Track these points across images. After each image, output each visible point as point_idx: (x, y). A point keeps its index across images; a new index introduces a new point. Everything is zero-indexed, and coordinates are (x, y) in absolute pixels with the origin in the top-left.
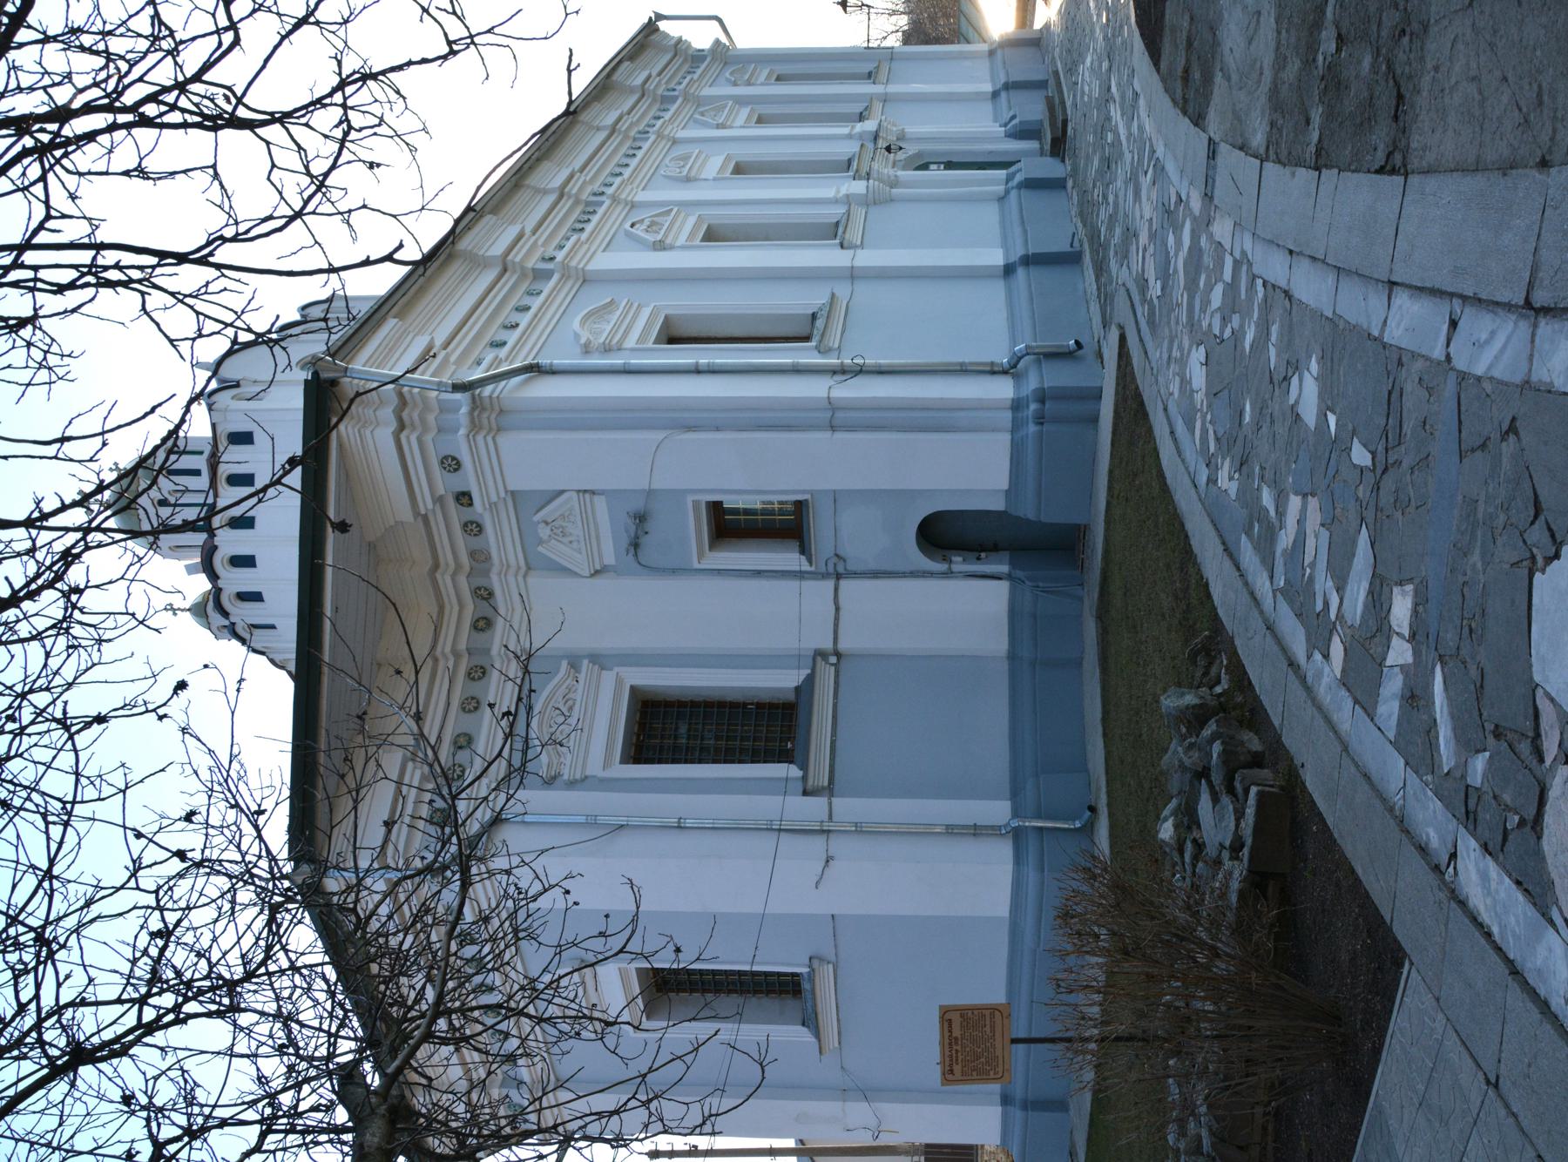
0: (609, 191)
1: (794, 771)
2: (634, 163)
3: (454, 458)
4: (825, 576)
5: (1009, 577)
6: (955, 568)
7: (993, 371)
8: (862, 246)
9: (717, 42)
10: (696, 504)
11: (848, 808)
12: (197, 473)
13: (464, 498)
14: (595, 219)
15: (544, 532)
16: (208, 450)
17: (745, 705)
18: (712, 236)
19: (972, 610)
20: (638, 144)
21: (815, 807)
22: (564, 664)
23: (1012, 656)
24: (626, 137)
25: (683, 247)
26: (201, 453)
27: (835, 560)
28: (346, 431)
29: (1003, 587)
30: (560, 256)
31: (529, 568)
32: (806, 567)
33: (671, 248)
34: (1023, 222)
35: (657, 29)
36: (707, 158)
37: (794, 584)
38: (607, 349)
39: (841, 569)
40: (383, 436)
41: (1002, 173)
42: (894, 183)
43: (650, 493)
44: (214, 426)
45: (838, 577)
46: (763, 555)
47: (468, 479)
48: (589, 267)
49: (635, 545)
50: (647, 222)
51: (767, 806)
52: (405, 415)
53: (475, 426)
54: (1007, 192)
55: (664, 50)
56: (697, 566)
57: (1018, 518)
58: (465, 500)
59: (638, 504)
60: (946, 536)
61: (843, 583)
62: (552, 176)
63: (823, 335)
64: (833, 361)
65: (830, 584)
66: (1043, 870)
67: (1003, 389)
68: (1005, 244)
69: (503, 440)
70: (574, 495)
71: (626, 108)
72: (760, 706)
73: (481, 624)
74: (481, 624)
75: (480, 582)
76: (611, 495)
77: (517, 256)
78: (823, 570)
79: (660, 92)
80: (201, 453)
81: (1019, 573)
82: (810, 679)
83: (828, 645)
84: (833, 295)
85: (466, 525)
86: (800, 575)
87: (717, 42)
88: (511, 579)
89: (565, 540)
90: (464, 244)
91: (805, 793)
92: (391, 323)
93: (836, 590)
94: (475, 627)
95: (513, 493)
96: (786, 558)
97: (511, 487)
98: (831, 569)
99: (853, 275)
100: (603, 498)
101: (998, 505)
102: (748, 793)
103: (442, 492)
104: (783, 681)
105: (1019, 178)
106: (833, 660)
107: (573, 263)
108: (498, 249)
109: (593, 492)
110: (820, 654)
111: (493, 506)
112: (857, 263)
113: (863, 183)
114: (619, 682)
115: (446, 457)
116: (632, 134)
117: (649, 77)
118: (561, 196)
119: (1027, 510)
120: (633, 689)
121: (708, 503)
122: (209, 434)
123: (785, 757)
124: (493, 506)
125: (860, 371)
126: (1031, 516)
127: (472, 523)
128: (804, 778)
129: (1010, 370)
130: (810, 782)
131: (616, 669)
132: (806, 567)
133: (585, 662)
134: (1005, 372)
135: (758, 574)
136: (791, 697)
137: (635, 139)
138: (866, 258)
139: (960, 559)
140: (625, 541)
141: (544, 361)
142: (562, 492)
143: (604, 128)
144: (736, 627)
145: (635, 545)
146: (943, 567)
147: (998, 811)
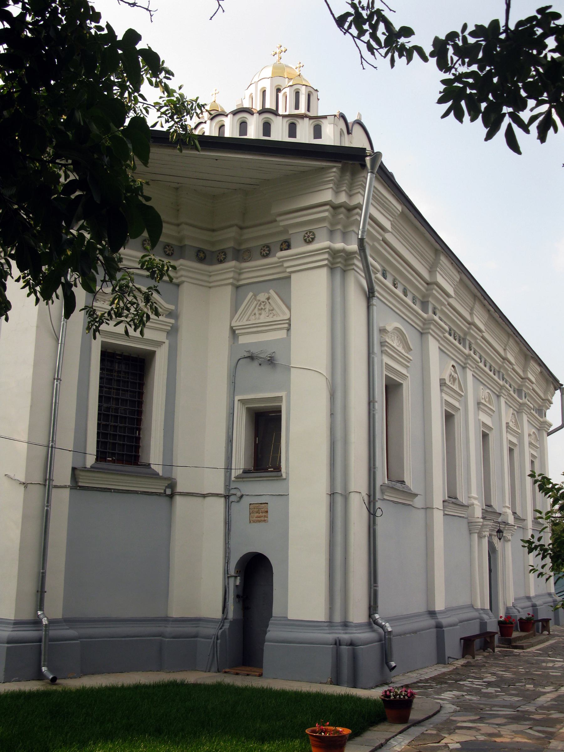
0: (472, 353)
1: (91, 460)
2: (487, 369)
3: (313, 239)
4: (227, 486)
5: (225, 619)
6: (232, 580)
7: (373, 608)
8: (445, 515)
9: (550, 425)
10: (280, 399)
11: (62, 499)
12: (297, 107)
13: (286, 245)
14: (456, 343)
15: (262, 297)
16: (311, 114)
17: (139, 429)
18: (449, 417)
19: (201, 590)
20: (497, 374)
21: (62, 475)
22: (172, 307)
23: (166, 620)
24: (500, 367)
25: (442, 398)
26: (309, 110)
27: (239, 494)
28: (334, 171)
29: (218, 615)
30: (436, 318)
31: (238, 287)
32: (234, 474)
33: (442, 391)
34: (461, 622)
35: (556, 390)
36: (490, 416)
37: (222, 464)
38: (383, 344)
39: (232, 498)
40: (327, 196)
41: (487, 607)
42: (480, 537)
43: (288, 368)
44: (325, 117)
45: (227, 497)
46: (441, 483)
47: (298, 249)
48: (430, 338)
49: (252, 358)
50: (456, 376)
51: (66, 438)
52: (343, 210)
53: (334, 254)
54: (477, 610)
55: (545, 393)
56: (237, 398)
57: (267, 626)
58: (284, 246)
59: (280, 360)
60: (253, 575)
61: (222, 500)
62: (480, 319)
63: (392, 488)
64: (378, 495)
65: (221, 491)
66: (8, 642)
67: (358, 614)
68: (448, 610)
69: (324, 271)
70: (287, 317)
71: (516, 367)
72: (138, 439)
73: (202, 255)
74: (202, 255)
75: (230, 255)
76: (286, 343)
77: (436, 292)
78: (233, 485)
79: (524, 389)
80: (309, 110)
81: (227, 625)
82: (155, 475)
83: (179, 489)
84: (416, 495)
85: (268, 247)
86: (228, 469)
87: (550, 425)
88: (231, 275)
89: (256, 311)
90: (443, 260)
91: (74, 469)
92: (399, 207)
93: (217, 495)
94: (200, 251)
95: (289, 277)
96: (241, 460)
97: (293, 276)
98: (233, 492)
99: (428, 509)
100: (285, 336)
101: (276, 610)
102: (76, 429)
103: (291, 232)
104: (154, 455)
105: (485, 617)
106: (169, 492)
107: (432, 327)
108: (440, 280)
109: (289, 330)
110: (172, 485)
111: (281, 264)
112: (435, 511)
113: (480, 515)
114: (159, 344)
115: (314, 234)
116: (502, 370)
117: (532, 383)
118: (469, 324)
119: (273, 632)
120: (154, 353)
121: (280, 407)
122: (320, 114)
123: (101, 456)
124: (281, 264)
125: (372, 514)
126: (269, 635)
127: (269, 251)
128: (85, 469)
129: (372, 623)
130: (81, 473)
131: (167, 342)
132: (234, 474)
133: (172, 321)
134: (370, 616)
135: (230, 441)
136: (143, 460)
137: (499, 372)
138: (438, 517)
139: (238, 583)
140: (255, 350)
141: (375, 301)
142: (290, 309)
143: (505, 353)
144: (195, 428)
145: (252, 358)
146: (232, 572)
147: (55, 608)
